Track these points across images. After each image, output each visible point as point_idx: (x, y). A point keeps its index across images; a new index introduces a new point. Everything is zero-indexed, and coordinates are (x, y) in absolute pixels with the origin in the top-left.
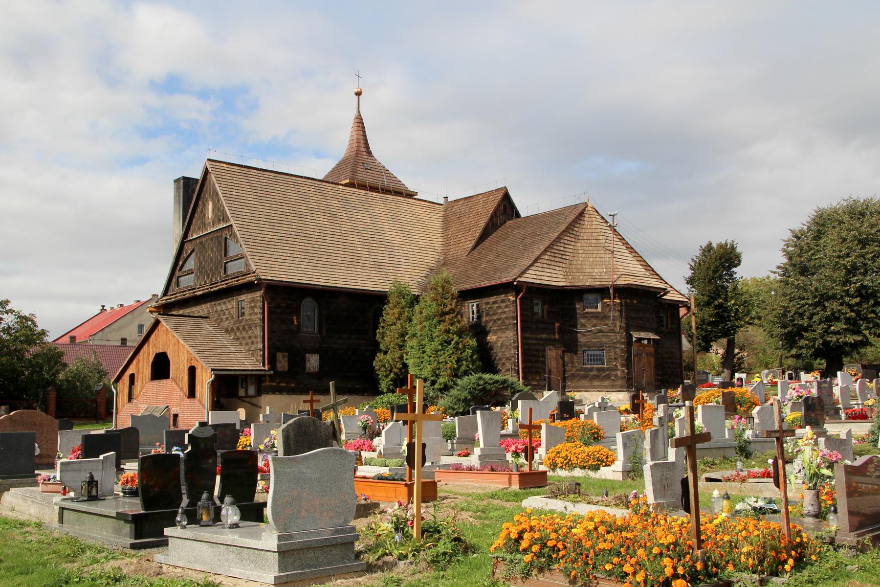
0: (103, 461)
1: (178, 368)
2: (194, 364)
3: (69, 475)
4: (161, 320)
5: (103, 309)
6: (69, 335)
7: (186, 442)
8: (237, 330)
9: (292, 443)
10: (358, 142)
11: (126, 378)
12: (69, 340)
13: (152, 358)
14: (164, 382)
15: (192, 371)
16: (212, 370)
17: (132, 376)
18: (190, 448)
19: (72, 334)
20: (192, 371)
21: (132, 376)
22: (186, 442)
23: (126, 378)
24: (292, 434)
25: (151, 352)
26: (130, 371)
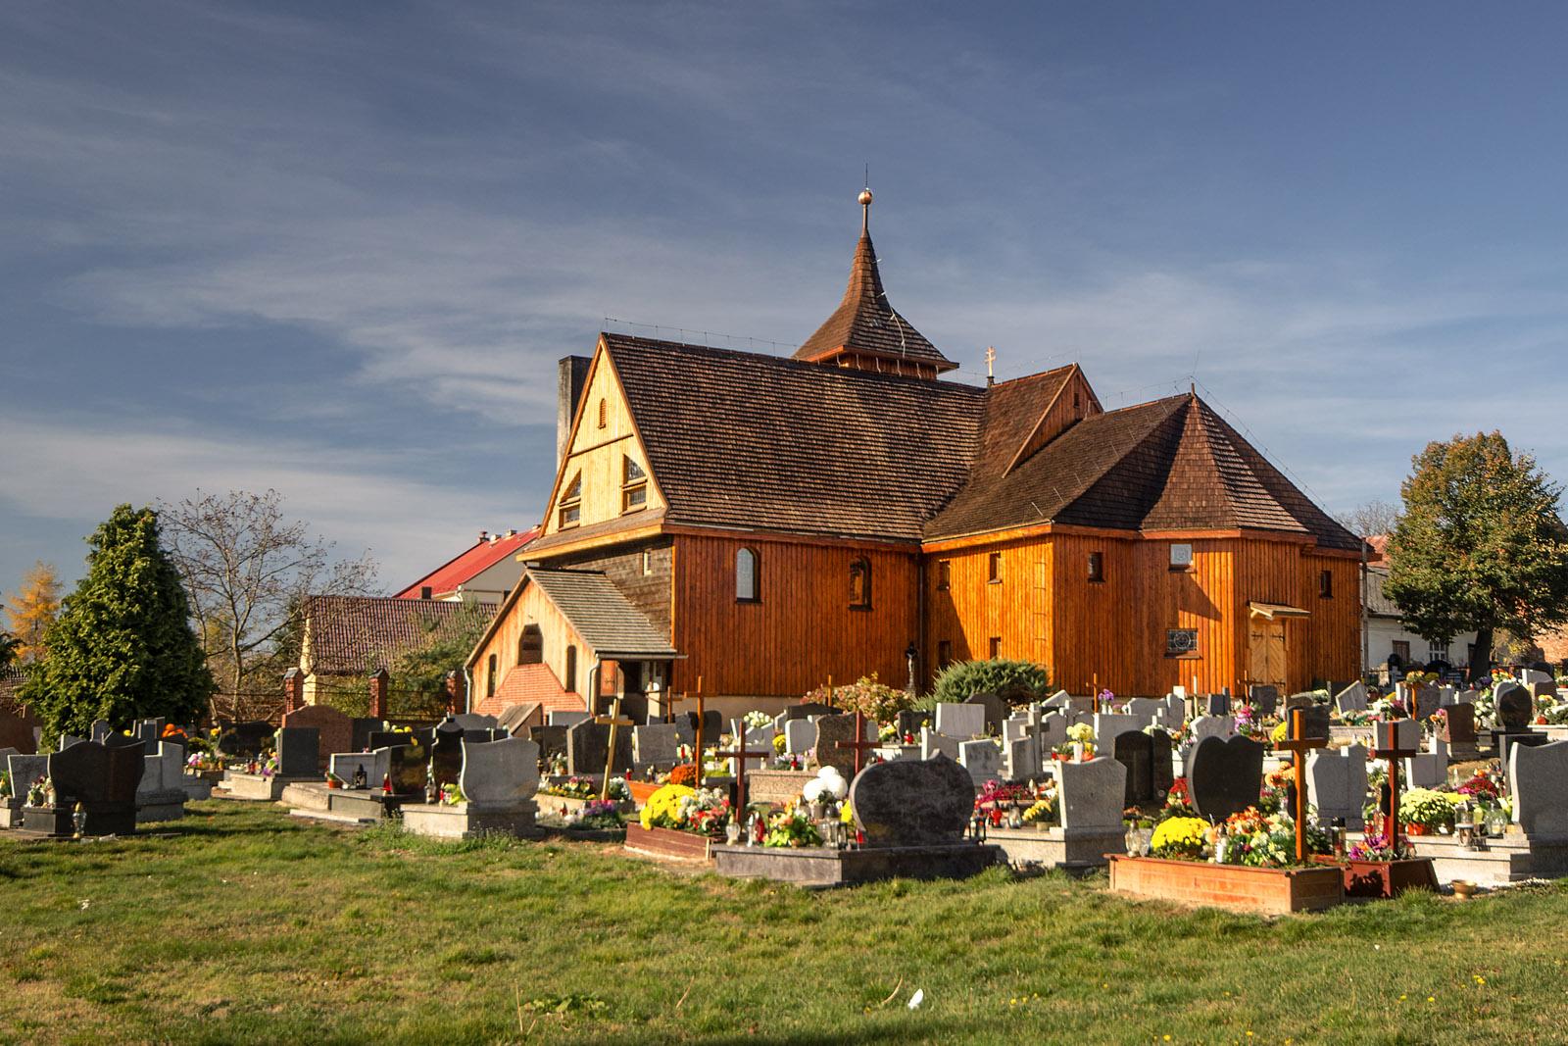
0: (376, 756)
1: (554, 652)
2: (574, 643)
3: (342, 768)
4: (531, 577)
5: (484, 540)
6: (420, 586)
7: (434, 736)
8: (643, 596)
9: (583, 746)
10: (865, 283)
11: (485, 661)
12: (421, 592)
13: (521, 630)
14: (534, 667)
15: (572, 652)
16: (597, 652)
17: (493, 659)
18: (437, 741)
19: (425, 584)
20: (572, 652)
21: (493, 659)
22: (434, 736)
23: (485, 661)
24: (583, 736)
25: (520, 624)
26: (491, 650)
